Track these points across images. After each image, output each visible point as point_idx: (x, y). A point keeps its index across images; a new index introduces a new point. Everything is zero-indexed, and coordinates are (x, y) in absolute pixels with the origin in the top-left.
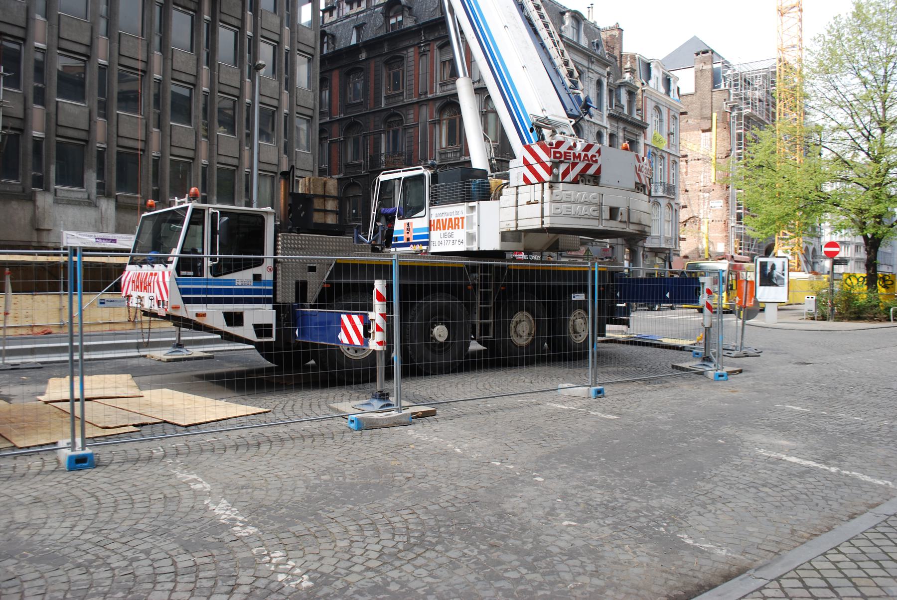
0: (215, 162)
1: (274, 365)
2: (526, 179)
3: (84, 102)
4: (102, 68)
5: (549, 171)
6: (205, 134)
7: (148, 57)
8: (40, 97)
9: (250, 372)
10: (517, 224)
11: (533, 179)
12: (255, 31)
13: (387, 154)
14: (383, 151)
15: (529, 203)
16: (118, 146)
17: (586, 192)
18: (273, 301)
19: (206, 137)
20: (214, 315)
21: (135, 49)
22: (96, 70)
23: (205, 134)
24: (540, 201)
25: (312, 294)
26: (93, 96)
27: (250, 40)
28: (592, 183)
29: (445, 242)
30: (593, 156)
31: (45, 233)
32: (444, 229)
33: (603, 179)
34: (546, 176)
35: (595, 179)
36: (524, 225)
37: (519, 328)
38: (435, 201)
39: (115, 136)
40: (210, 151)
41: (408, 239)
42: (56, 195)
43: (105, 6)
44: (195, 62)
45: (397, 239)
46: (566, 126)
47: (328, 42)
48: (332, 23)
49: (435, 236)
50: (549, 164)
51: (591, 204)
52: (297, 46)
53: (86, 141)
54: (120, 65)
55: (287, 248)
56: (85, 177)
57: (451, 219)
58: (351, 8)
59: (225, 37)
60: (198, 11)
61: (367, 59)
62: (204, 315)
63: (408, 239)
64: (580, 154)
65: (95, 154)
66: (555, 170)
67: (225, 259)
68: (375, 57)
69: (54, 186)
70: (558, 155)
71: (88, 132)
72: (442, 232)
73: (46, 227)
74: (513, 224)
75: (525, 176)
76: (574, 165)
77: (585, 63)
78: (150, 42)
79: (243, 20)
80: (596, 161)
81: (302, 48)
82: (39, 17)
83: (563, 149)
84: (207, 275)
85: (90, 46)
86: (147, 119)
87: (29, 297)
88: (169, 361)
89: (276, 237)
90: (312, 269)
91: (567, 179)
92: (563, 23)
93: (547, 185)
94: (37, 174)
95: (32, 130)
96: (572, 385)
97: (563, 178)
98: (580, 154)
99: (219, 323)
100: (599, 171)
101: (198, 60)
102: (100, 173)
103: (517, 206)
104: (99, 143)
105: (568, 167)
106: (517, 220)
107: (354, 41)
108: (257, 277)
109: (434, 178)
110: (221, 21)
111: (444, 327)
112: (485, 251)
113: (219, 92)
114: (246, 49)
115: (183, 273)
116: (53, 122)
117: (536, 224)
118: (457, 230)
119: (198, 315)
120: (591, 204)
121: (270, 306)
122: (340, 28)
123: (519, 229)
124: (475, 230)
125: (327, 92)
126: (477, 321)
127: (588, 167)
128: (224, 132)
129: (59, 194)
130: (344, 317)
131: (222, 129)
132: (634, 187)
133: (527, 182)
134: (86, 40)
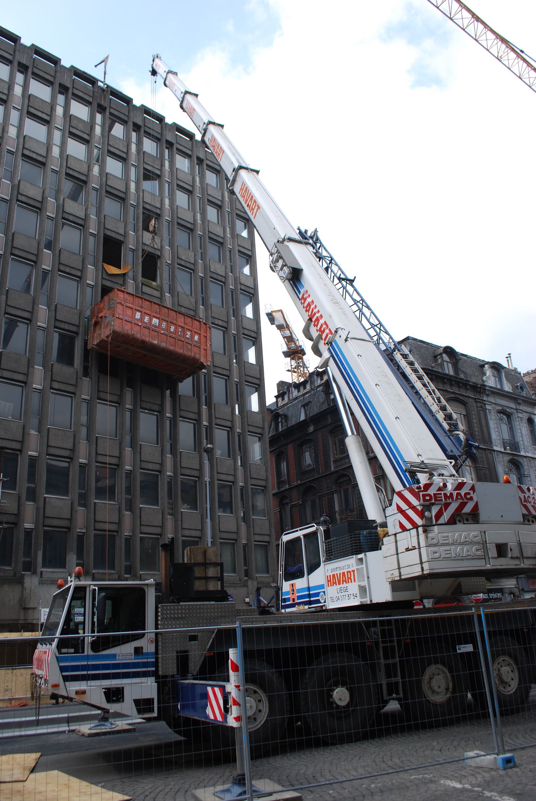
0: (180, 535)
1: (182, 738)
2: (402, 526)
3: (68, 496)
4: (82, 467)
5: (421, 515)
6: (171, 511)
7: (120, 453)
8: (32, 495)
9: (158, 747)
10: (400, 573)
11: (408, 525)
12: (210, 421)
13: (341, 512)
14: (337, 508)
15: (408, 550)
16: (95, 530)
17: (465, 532)
18: (155, 674)
19: (172, 514)
20: (95, 691)
21: (108, 448)
22: (77, 468)
23: (171, 511)
24: (417, 547)
25: (194, 665)
26: (75, 490)
27: (206, 429)
28: (471, 521)
29: (340, 597)
30: (466, 494)
31: (30, 612)
32: (339, 584)
33: (483, 517)
34: (418, 521)
35: (474, 517)
36: (407, 573)
37: (434, 683)
38: (331, 556)
39: (93, 521)
40: (176, 526)
41: (294, 600)
42: (41, 576)
43: (86, 417)
44: (160, 452)
45: (285, 600)
46: (444, 467)
47: (281, 422)
48: (284, 405)
49: (332, 591)
50: (419, 508)
51: (472, 543)
52: (247, 428)
53: (69, 528)
54: (97, 462)
55: (166, 618)
56: (67, 558)
57: (344, 573)
58: (299, 391)
59: (186, 430)
60: (161, 411)
61: (315, 431)
62: (84, 692)
63: (294, 600)
64: (451, 494)
65: (75, 538)
66: (427, 514)
67: (102, 636)
68: (320, 429)
69: (40, 569)
70: (428, 498)
71: (70, 520)
72: (338, 586)
73: (32, 606)
74: (396, 573)
75: (400, 523)
76: (447, 505)
77: (513, 405)
78: (122, 440)
79: (199, 413)
80: (471, 499)
81: (252, 429)
82: (33, 432)
83: (432, 491)
84: (88, 651)
85: (73, 450)
86: (120, 504)
87: (10, 671)
88: (90, 735)
89: (157, 608)
90: (193, 638)
91: (441, 521)
92: (484, 374)
93: (420, 529)
94: (27, 559)
95: (24, 523)
96: (483, 753)
97: (436, 521)
98: (451, 494)
99: (100, 699)
100: (476, 507)
101: (162, 450)
102: (80, 554)
103: (397, 554)
104: (80, 528)
105: (441, 508)
106: (399, 568)
107: (303, 418)
108: (138, 651)
109: (327, 533)
110: (180, 417)
111: (344, 690)
112: (378, 604)
113: (182, 475)
114: (203, 436)
115: (64, 650)
116: (42, 515)
117: (416, 571)
118: (344, 585)
119: (77, 693)
120: (472, 543)
121: (153, 679)
122: (291, 409)
123: (403, 577)
124: (365, 583)
125: (285, 463)
126: (384, 682)
127: (462, 505)
128: (187, 509)
129: (44, 576)
130: (209, 689)
131: (185, 506)
132: (522, 520)
133: (403, 528)
134: (70, 446)
